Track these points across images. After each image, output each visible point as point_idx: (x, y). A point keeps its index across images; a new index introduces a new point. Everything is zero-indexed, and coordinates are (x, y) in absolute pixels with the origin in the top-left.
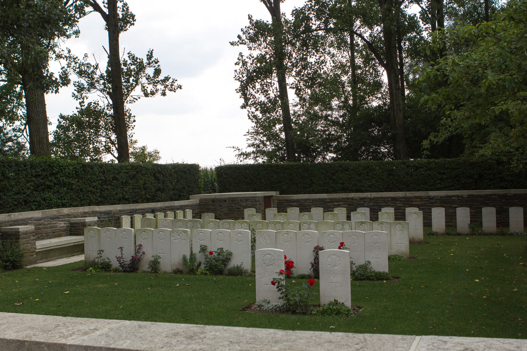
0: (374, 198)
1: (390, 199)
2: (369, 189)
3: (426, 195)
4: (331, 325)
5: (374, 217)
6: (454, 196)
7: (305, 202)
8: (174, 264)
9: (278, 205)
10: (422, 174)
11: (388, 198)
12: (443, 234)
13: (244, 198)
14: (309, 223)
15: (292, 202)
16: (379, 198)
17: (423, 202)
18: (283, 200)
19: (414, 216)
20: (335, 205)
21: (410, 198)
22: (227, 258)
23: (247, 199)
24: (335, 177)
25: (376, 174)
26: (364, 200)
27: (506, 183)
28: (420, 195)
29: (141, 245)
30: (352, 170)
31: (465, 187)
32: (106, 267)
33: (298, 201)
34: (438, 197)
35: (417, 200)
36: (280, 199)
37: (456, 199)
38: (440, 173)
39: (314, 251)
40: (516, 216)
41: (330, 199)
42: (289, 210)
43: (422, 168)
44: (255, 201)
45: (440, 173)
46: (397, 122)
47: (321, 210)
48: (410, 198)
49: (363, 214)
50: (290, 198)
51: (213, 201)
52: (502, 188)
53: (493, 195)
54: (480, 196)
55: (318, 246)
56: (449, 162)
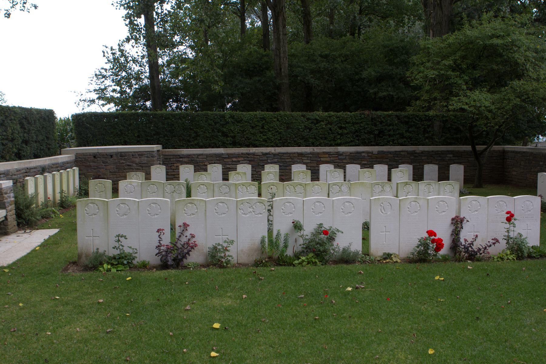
0: (278, 154)
1: (296, 155)
2: (264, 143)
3: (336, 151)
5: (418, 176)
6: (363, 152)
7: (198, 158)
8: (242, 251)
9: (163, 162)
10: (323, 128)
11: (295, 153)
13: (137, 152)
14: (340, 185)
16: (284, 153)
17: (332, 159)
18: (170, 155)
20: (233, 161)
21: (318, 154)
22: (329, 235)
23: (208, 156)
25: (273, 127)
26: (268, 156)
28: (328, 151)
29: (186, 225)
30: (246, 122)
31: (365, 143)
32: (123, 261)
33: (188, 156)
34: (347, 152)
35: (324, 156)
36: (167, 154)
37: (366, 155)
39: (452, 223)
41: (228, 154)
42: (209, 167)
43: (323, 121)
44: (152, 157)
45: (341, 128)
46: (283, 70)
47: (192, 167)
48: (318, 154)
49: (403, 173)
50: (179, 153)
51: (95, 157)
52: (402, 145)
53: (402, 151)
56: (351, 116)
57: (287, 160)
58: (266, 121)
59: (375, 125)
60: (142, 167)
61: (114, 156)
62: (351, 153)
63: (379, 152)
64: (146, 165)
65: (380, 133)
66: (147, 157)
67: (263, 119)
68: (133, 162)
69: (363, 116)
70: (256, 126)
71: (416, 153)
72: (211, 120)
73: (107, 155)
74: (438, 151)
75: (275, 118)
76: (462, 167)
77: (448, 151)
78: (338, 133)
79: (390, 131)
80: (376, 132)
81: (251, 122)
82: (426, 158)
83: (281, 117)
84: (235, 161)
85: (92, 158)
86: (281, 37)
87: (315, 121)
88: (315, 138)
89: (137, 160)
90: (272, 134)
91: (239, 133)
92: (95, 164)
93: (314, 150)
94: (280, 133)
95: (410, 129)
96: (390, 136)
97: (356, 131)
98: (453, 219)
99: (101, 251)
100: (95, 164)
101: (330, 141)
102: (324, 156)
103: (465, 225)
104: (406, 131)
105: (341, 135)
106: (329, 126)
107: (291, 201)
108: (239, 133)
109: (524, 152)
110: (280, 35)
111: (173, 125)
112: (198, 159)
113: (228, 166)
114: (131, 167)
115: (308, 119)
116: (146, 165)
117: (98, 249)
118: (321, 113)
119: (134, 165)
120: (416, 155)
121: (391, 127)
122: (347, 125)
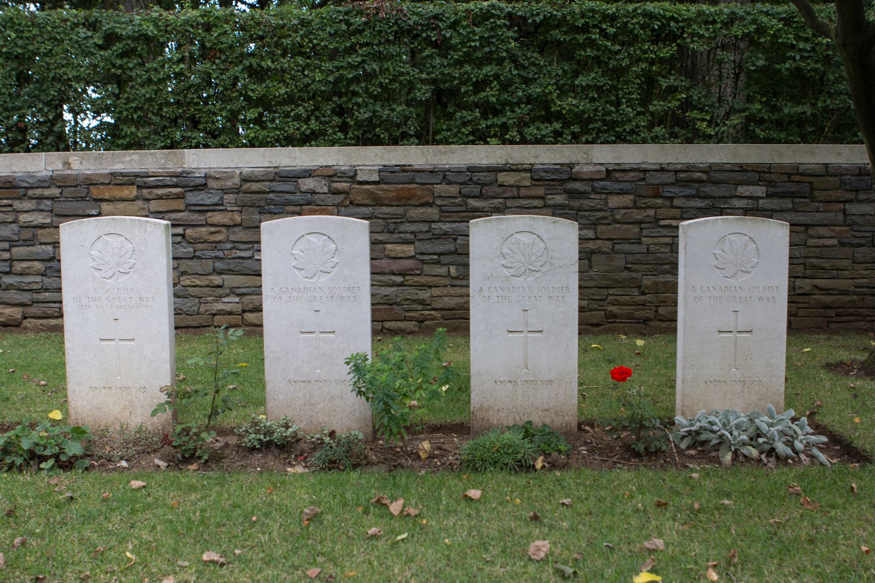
1: (525, 179)
6: (309, 173)
12: (142, 447)
21: (89, 182)
27: (557, 126)
28: (135, 168)
34: (227, 175)
38: (257, 74)
40: (734, 280)
45: (257, 74)
54: (444, 175)
62: (245, 180)
63: (387, 174)
65: (438, 93)
74: (689, 169)
76: (773, 238)
77: (742, 168)
78: (247, 98)
79: (480, 86)
80: (423, 93)
82: (627, 199)
93: (67, 164)
95: (582, 81)
105: (263, 102)
115: (111, 38)
120: (577, 185)
121: (489, 70)
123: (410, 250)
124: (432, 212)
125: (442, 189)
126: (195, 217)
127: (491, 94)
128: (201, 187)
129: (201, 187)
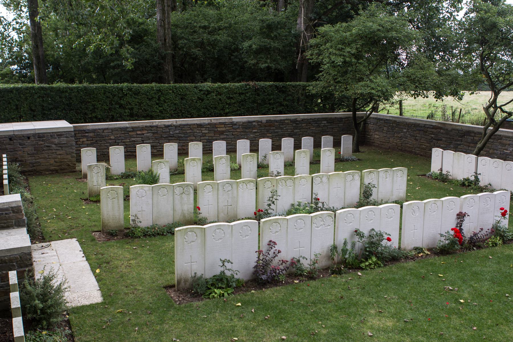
1: (196, 126)
4: (462, 303)
7: (103, 132)
10: (214, 99)
11: (194, 124)
13: (55, 133)
15: (86, 133)
17: (227, 128)
19: (328, 153)
20: (137, 134)
21: (215, 124)
24: (122, 102)
26: (170, 128)
34: (240, 122)
35: (220, 126)
38: (229, 98)
41: (132, 128)
43: (213, 92)
45: (229, 98)
46: (167, 41)
51: (10, 139)
55: (461, 213)
56: (238, 87)
57: (188, 131)
58: (162, 93)
59: (258, 95)
60: (62, 147)
61: (32, 137)
63: (268, 121)
64: (66, 145)
66: (66, 137)
67: (159, 91)
68: (52, 143)
69: (248, 87)
70: (153, 98)
71: (297, 121)
72: (110, 92)
73: (23, 136)
75: (170, 89)
79: (270, 100)
81: (148, 94)
82: (305, 124)
83: (176, 89)
84: (139, 134)
85: (8, 141)
86: (166, 9)
87: (207, 93)
88: (206, 108)
89: (56, 141)
90: (168, 105)
91: (136, 105)
92: (11, 147)
94: (175, 104)
95: (287, 98)
96: (270, 104)
97: (242, 101)
98: (458, 215)
99: (199, 274)
100: (11, 147)
101: (220, 110)
102: (220, 126)
103: (466, 218)
104: (284, 99)
105: (229, 104)
106: (219, 97)
107: (352, 212)
108: (136, 105)
109: (387, 120)
110: (164, 6)
111: (71, 98)
112: (103, 134)
113: (133, 139)
114: (51, 148)
115: (201, 90)
116: (66, 145)
117: (195, 273)
118: (209, 84)
119: (53, 146)
122: (234, 95)
123: (271, 135)
124: (274, 128)
125: (276, 124)
126: (235, 130)
127: (272, 101)
128: (235, 125)
129: (235, 125)
